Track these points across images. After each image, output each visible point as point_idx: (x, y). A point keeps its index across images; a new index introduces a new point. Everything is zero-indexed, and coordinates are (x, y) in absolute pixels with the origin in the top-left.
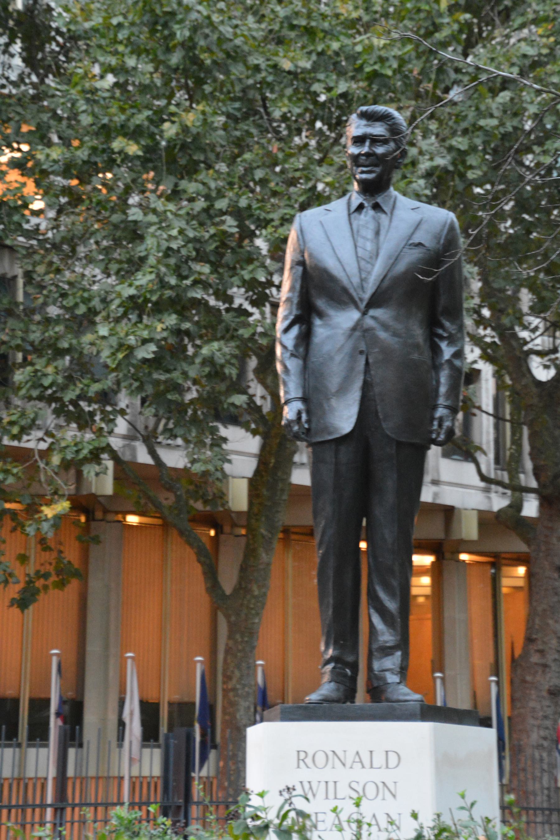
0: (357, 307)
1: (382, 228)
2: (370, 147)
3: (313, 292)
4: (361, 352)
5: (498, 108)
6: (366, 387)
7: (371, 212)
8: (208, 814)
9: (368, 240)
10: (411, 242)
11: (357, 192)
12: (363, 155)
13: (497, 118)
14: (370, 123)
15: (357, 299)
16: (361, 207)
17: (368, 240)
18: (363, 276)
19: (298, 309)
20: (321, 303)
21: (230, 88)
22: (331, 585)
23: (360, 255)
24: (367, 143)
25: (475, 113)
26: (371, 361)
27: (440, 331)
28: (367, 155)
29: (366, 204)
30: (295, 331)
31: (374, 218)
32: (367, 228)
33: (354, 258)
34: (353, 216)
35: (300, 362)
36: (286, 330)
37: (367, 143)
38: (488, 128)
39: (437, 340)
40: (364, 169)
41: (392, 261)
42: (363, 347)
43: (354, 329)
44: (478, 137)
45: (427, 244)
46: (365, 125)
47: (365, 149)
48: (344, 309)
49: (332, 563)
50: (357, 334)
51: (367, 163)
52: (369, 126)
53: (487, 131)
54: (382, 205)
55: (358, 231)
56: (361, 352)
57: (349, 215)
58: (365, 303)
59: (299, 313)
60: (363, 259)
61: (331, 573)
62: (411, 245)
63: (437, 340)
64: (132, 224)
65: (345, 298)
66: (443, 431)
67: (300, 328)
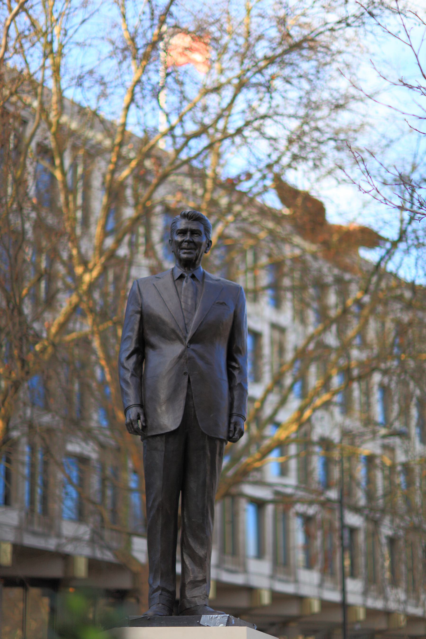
0: (182, 343)
3: (148, 332)
4: (185, 374)
6: (189, 397)
7: (190, 280)
8: (410, 187)
12: (186, 242)
16: (182, 277)
20: (153, 339)
21: (251, 242)
22: (159, 536)
24: (189, 234)
26: (191, 380)
27: (234, 364)
28: (189, 242)
29: (186, 275)
30: (134, 359)
35: (138, 380)
36: (129, 358)
37: (189, 234)
39: (231, 369)
40: (185, 251)
42: (186, 370)
43: (180, 357)
47: (188, 238)
49: (160, 522)
50: (182, 361)
56: (185, 374)
57: (174, 281)
61: (159, 527)
62: (217, 303)
63: (231, 369)
65: (173, 336)
66: (237, 432)
67: (137, 357)
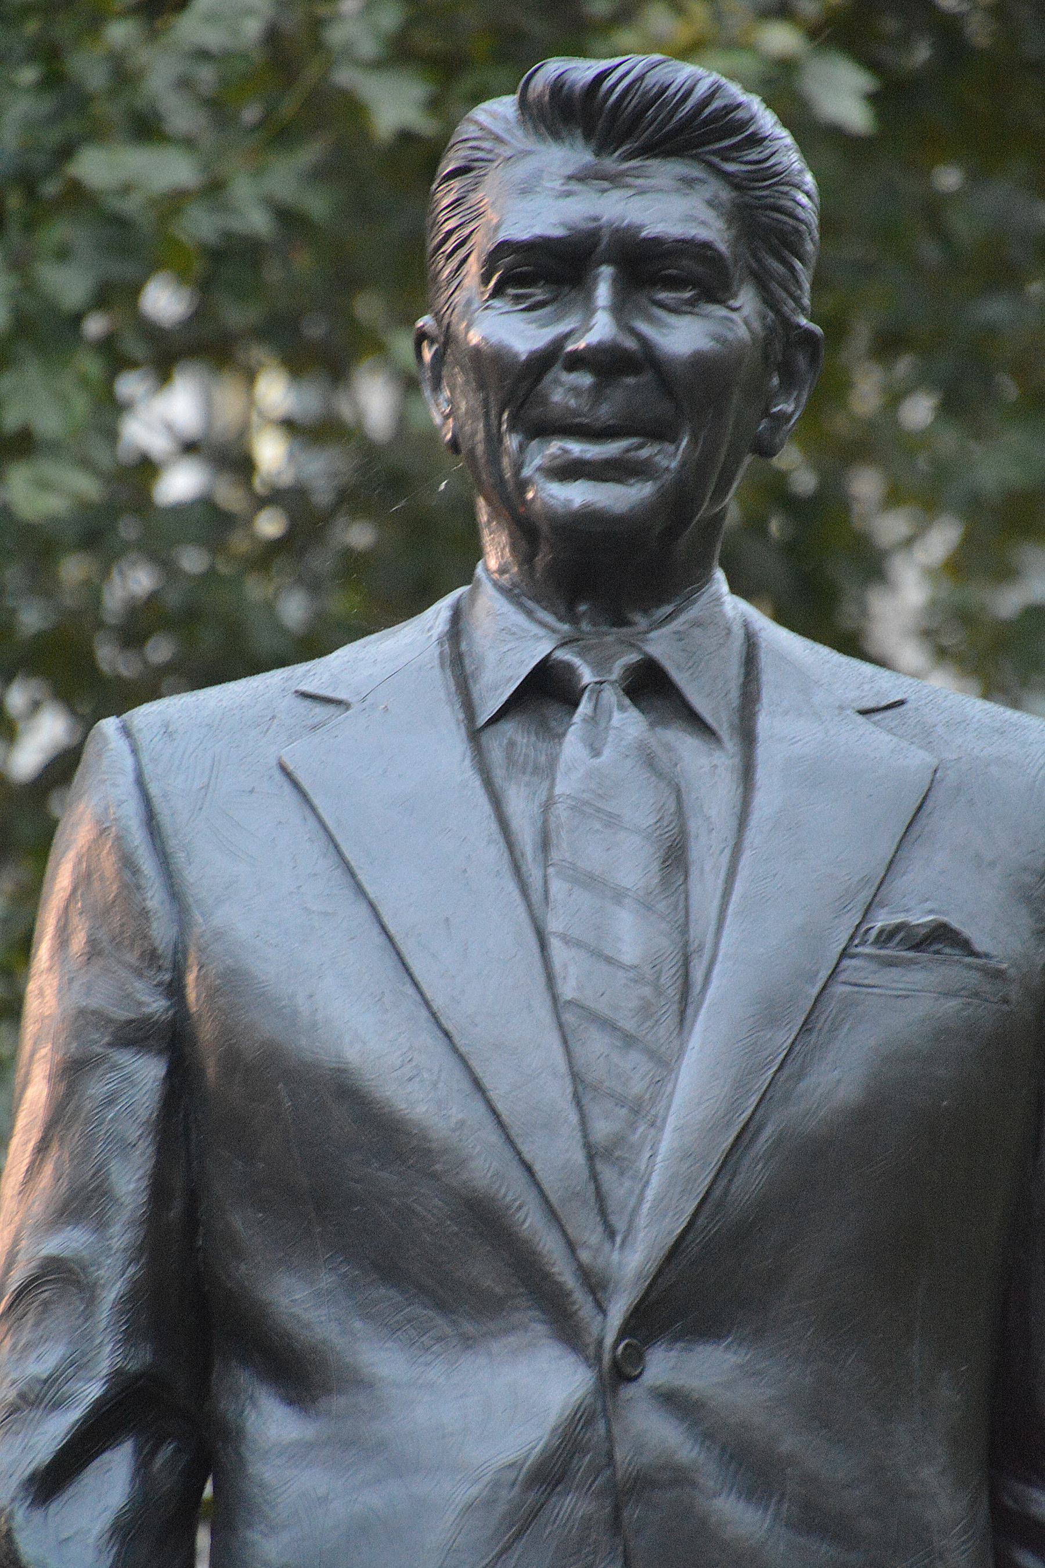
1: (695, 825)
2: (619, 309)
5: (185, 84)
9: (618, 896)
10: (882, 920)
11: (509, 593)
12: (576, 362)
13: (188, 143)
14: (610, 164)
15: (569, 1279)
17: (618, 896)
18: (602, 1129)
19: (129, 1338)
23: (568, 990)
25: (46, 105)
31: (649, 760)
32: (612, 821)
33: (543, 1012)
34: (485, 738)
38: (130, 206)
40: (577, 449)
41: (784, 1038)
44: (63, 254)
45: (981, 943)
46: (582, 177)
48: (468, 1342)
51: (605, 412)
52: (615, 180)
53: (120, 222)
54: (680, 678)
55: (545, 844)
57: (475, 735)
58: (618, 1310)
59: (141, 1358)
60: (607, 1025)
62: (886, 936)
64: (560, 731)
